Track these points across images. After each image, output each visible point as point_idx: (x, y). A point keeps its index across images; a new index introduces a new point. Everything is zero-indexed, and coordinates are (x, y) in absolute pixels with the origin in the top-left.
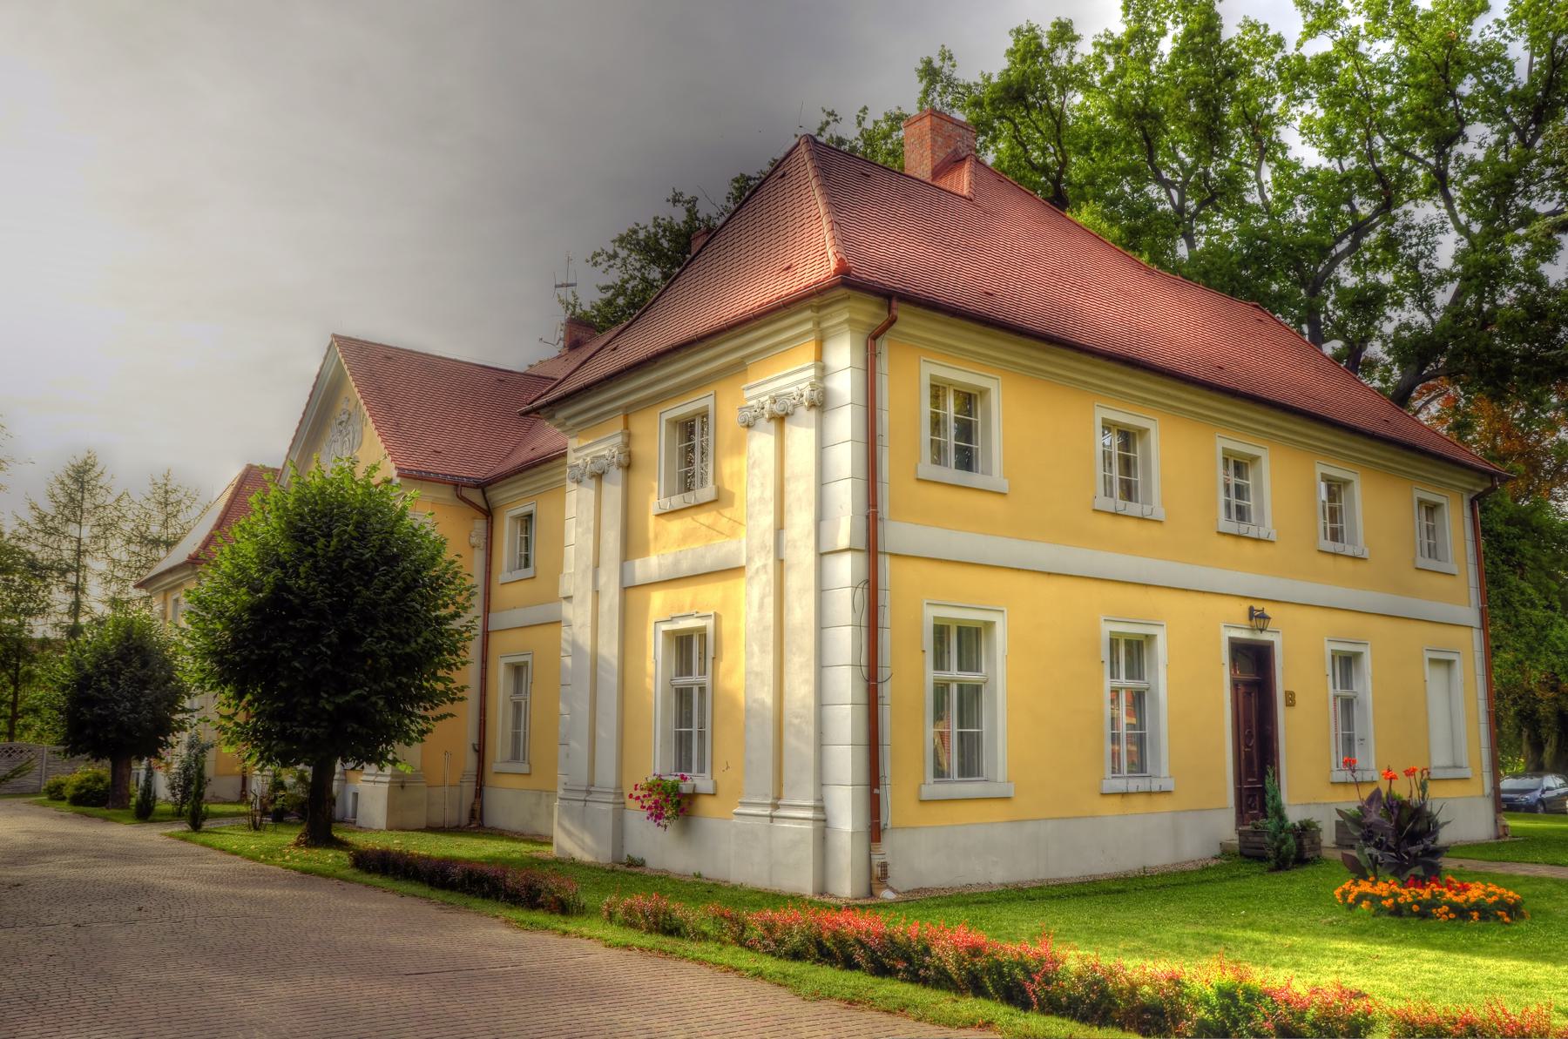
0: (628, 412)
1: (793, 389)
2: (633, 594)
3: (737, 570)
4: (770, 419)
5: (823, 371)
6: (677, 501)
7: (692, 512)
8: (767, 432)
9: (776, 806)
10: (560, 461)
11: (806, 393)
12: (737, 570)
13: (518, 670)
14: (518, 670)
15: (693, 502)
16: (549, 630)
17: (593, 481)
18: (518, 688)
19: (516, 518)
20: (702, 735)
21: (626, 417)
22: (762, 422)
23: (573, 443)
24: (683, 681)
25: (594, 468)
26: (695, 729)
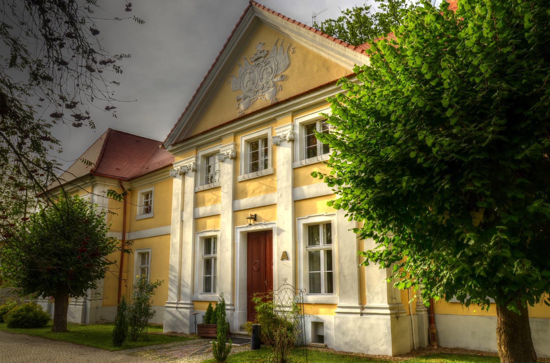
0: (236, 134)
1: (187, 164)
2: (201, 221)
3: (218, 215)
4: (180, 175)
5: (236, 145)
6: (251, 175)
7: (211, 191)
8: (230, 164)
9: (363, 308)
10: (169, 168)
11: (230, 153)
12: (218, 215)
13: (144, 256)
14: (144, 256)
15: (260, 175)
16: (167, 236)
17: (181, 177)
18: (143, 263)
19: (143, 193)
20: (215, 277)
21: (235, 136)
22: (178, 175)
23: (178, 159)
24: (208, 256)
25: (182, 171)
26: (212, 276)
